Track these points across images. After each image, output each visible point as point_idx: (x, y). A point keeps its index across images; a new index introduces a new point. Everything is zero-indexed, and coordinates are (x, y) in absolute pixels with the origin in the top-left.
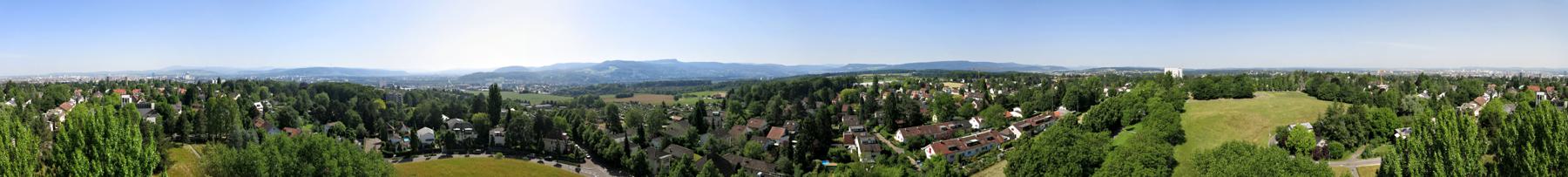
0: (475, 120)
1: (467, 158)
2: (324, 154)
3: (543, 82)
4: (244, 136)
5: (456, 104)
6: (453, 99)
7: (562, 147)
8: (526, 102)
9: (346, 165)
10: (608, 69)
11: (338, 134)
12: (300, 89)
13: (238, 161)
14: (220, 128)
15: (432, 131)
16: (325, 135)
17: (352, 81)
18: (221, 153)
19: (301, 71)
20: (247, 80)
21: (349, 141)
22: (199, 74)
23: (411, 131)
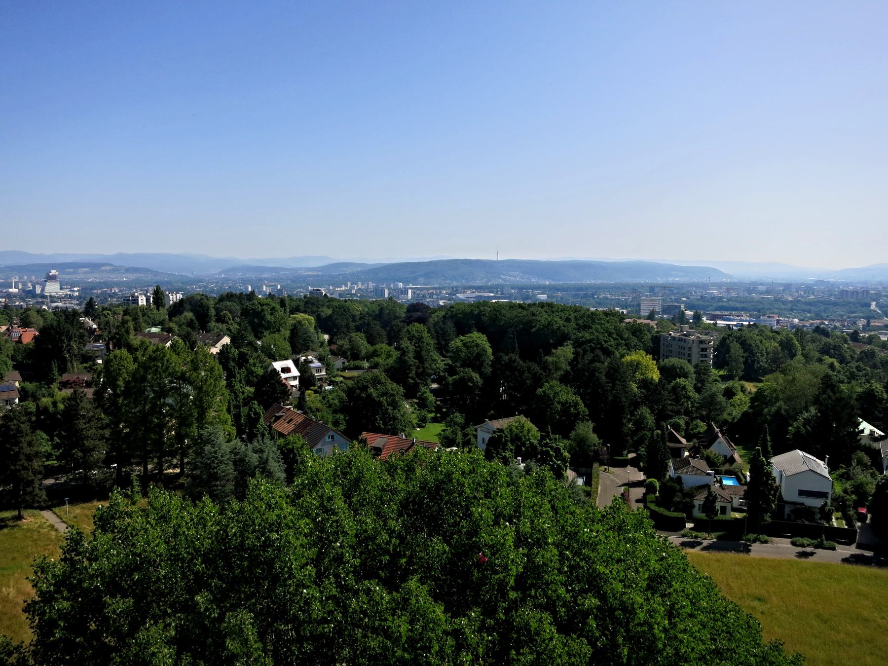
2: (476, 510)
4: (240, 463)
9: (541, 543)
11: (517, 453)
12: (409, 321)
13: (222, 538)
14: (159, 443)
15: (822, 467)
16: (479, 454)
17: (559, 298)
18: (164, 518)
19: (410, 271)
20: (251, 296)
21: (549, 474)
22: (93, 278)
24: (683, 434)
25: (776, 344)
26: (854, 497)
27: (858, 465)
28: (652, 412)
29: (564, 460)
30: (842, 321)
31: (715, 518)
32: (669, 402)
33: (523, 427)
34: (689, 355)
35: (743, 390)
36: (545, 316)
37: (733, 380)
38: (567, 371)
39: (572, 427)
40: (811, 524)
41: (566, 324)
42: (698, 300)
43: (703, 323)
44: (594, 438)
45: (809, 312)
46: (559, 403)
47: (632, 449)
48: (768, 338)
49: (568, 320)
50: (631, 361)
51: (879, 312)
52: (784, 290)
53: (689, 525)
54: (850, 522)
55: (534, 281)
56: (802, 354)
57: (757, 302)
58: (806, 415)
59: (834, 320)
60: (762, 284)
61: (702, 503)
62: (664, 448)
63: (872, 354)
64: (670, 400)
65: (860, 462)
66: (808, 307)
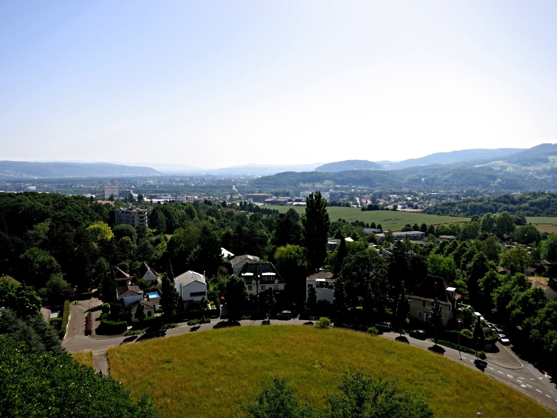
0: (281, 258)
1: (266, 326)
3: (404, 189)
5: (245, 228)
6: (242, 219)
7: (446, 314)
8: (373, 226)
10: (546, 161)
15: (202, 278)
23: (163, 280)
24: (128, 271)
25: (183, 211)
26: (219, 291)
27: (220, 274)
28: (108, 259)
29: (38, 303)
30: (219, 196)
31: (144, 320)
32: (118, 253)
33: (7, 284)
34: (133, 221)
35: (166, 239)
36: (29, 201)
37: (160, 234)
38: (44, 239)
39: (48, 278)
40: (198, 311)
41: (46, 206)
42: (142, 187)
43: (144, 201)
44: (64, 283)
45: (203, 192)
46: (37, 262)
47: (94, 286)
48: (179, 208)
49: (47, 204)
50: (94, 229)
51: (237, 191)
52: (190, 180)
53: (129, 328)
54: (217, 307)
55: (25, 176)
56: (198, 216)
57: (176, 187)
58: (195, 250)
59: (215, 196)
60: (178, 177)
61: (135, 312)
62: (114, 282)
63: (231, 214)
64: (119, 251)
65: (221, 272)
66: (202, 190)
